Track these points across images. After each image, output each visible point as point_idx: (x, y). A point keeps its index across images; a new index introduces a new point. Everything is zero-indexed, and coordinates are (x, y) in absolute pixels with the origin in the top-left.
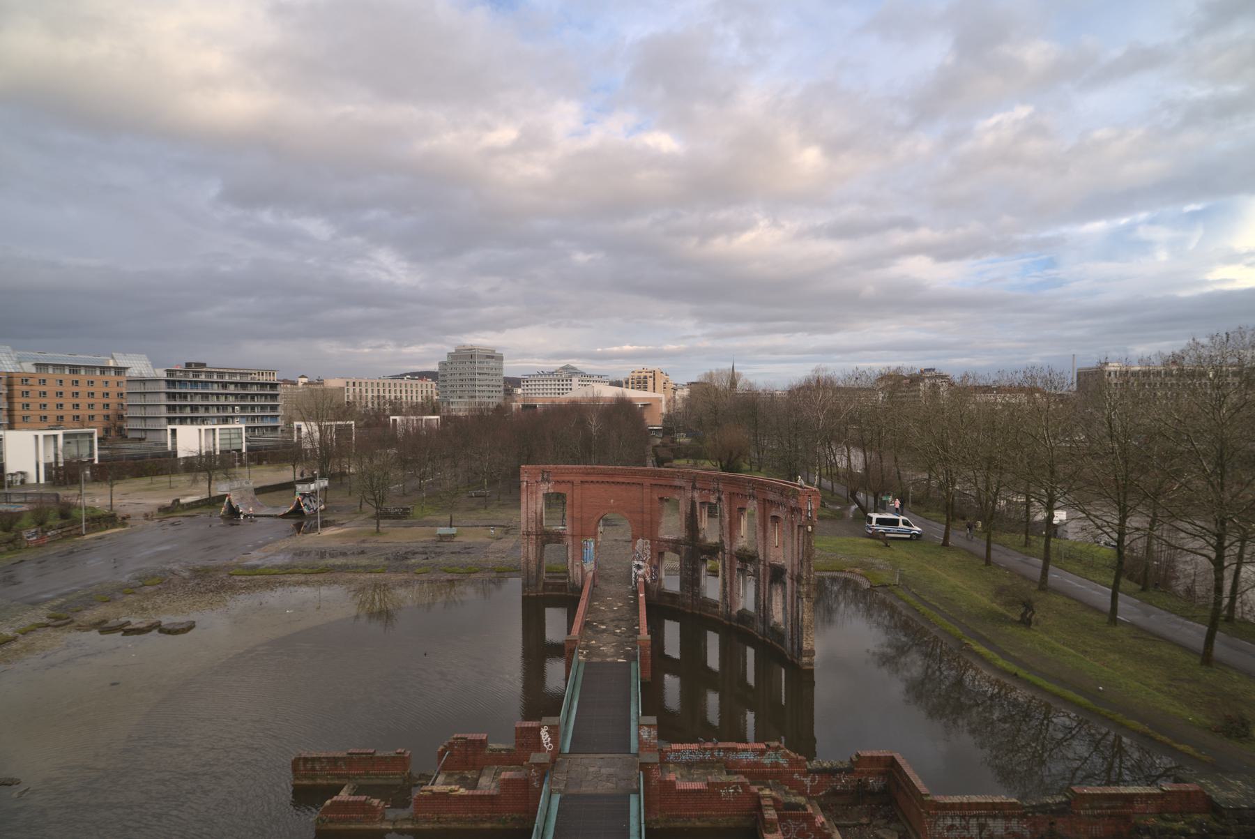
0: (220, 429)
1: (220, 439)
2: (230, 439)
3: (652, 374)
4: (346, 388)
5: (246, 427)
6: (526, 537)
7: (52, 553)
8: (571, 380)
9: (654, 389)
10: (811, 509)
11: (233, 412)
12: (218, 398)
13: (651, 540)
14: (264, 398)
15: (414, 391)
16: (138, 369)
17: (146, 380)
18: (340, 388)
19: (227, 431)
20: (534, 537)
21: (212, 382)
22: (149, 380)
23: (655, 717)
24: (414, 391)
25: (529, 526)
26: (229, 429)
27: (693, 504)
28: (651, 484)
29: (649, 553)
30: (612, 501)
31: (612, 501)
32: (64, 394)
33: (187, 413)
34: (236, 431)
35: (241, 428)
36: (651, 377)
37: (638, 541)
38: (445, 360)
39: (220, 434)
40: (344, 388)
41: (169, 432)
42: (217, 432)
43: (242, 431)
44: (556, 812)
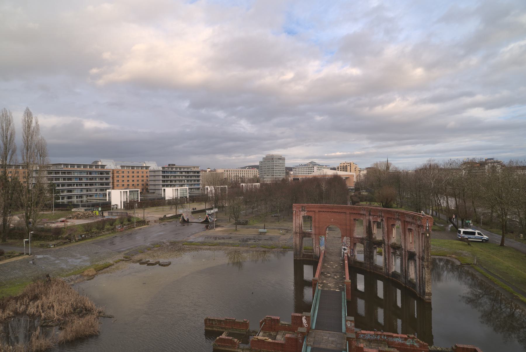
3: (349, 164)
8: (313, 168)
11: (184, 182)
18: (222, 172)
19: (182, 190)
20: (299, 234)
26: (183, 189)
27: (370, 222)
28: (350, 213)
31: (332, 220)
33: (169, 183)
35: (187, 189)
36: (349, 166)
39: (180, 191)
40: (223, 172)
41: (163, 190)
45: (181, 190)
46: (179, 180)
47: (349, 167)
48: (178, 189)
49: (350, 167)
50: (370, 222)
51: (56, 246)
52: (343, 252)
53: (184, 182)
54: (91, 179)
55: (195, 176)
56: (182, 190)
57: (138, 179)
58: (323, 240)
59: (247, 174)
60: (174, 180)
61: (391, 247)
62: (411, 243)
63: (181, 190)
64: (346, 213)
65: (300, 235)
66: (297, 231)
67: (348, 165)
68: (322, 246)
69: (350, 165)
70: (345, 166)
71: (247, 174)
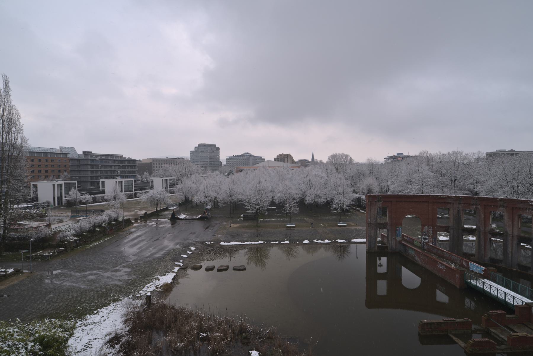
0: (124, 181)
1: (124, 186)
2: (128, 185)
3: (287, 156)
4: (153, 163)
5: (134, 180)
6: (370, 226)
7: (445, 263)
8: (249, 159)
9: (288, 160)
10: (17, 200)
11: (118, 174)
12: (111, 167)
13: (433, 227)
14: (134, 167)
15: (158, 164)
16: (72, 154)
17: (80, 159)
18: (151, 163)
19: (127, 182)
20: (374, 226)
21: (109, 160)
22: (82, 159)
23: (378, 281)
24: (158, 164)
25: (372, 221)
26: (128, 181)
27: (459, 211)
28: (433, 202)
29: (432, 232)
30: (411, 209)
31: (411, 209)
32: (42, 166)
33: (109, 174)
34: (130, 182)
35: (132, 181)
36: (286, 157)
37: (425, 227)
38: (193, 150)
39: (124, 183)
40: (152, 163)
41: (101, 183)
42: (123, 182)
43: (132, 182)
44: (438, 322)
45: (125, 182)
46: (110, 170)
47: (287, 158)
48: (121, 182)
49: (288, 158)
50: (459, 211)
51: (52, 257)
52: (423, 242)
53: (118, 174)
54: (229, 162)
55: (131, 166)
56: (127, 182)
57: (53, 169)
58: (400, 231)
59: (159, 164)
60: (104, 170)
61: (489, 233)
62: (519, 228)
63: (125, 182)
64: (428, 202)
65: (375, 227)
66: (372, 223)
67: (285, 156)
68: (399, 237)
69: (288, 156)
70: (282, 157)
71: (159, 164)
